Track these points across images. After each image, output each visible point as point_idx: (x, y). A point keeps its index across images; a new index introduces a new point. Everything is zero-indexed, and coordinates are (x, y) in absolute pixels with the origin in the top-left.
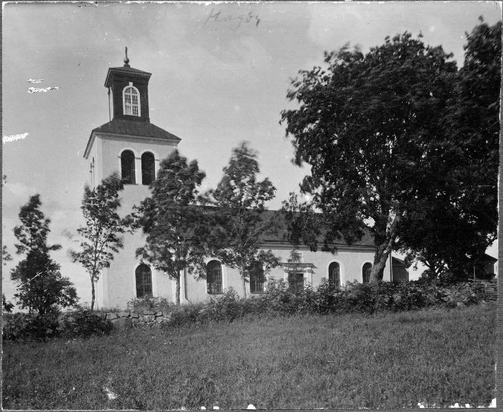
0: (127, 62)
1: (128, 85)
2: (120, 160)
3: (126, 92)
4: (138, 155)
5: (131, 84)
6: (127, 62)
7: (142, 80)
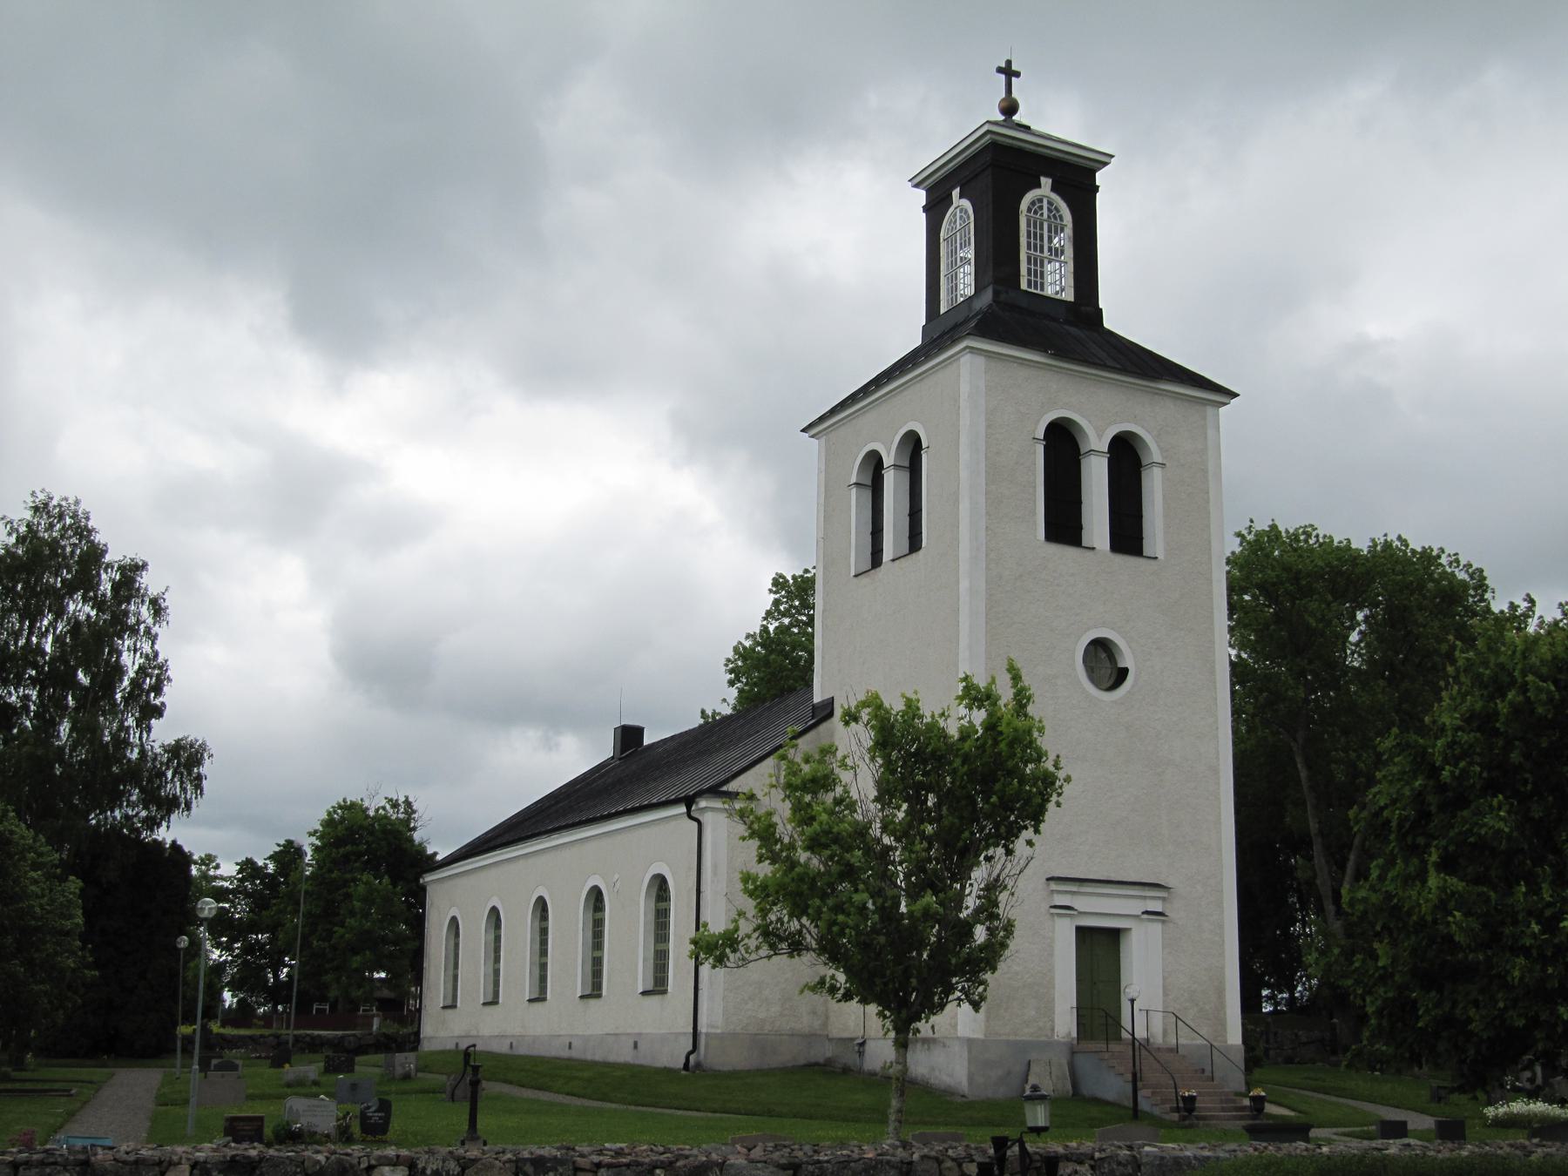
0: (1010, 108)
1: (1039, 186)
2: (1040, 449)
3: (1029, 210)
4: (1096, 439)
5: (1046, 182)
6: (1010, 108)
7: (1076, 178)
